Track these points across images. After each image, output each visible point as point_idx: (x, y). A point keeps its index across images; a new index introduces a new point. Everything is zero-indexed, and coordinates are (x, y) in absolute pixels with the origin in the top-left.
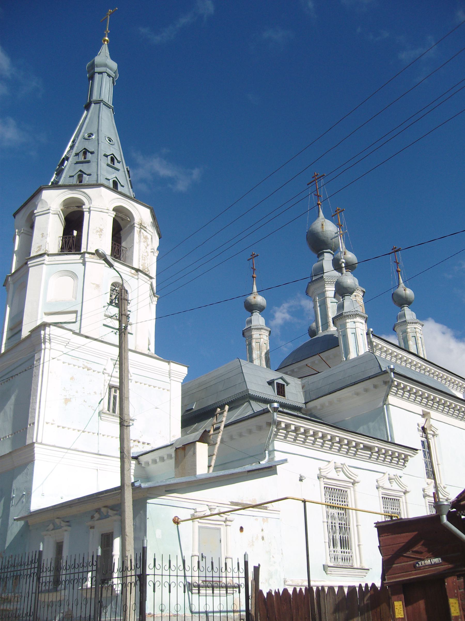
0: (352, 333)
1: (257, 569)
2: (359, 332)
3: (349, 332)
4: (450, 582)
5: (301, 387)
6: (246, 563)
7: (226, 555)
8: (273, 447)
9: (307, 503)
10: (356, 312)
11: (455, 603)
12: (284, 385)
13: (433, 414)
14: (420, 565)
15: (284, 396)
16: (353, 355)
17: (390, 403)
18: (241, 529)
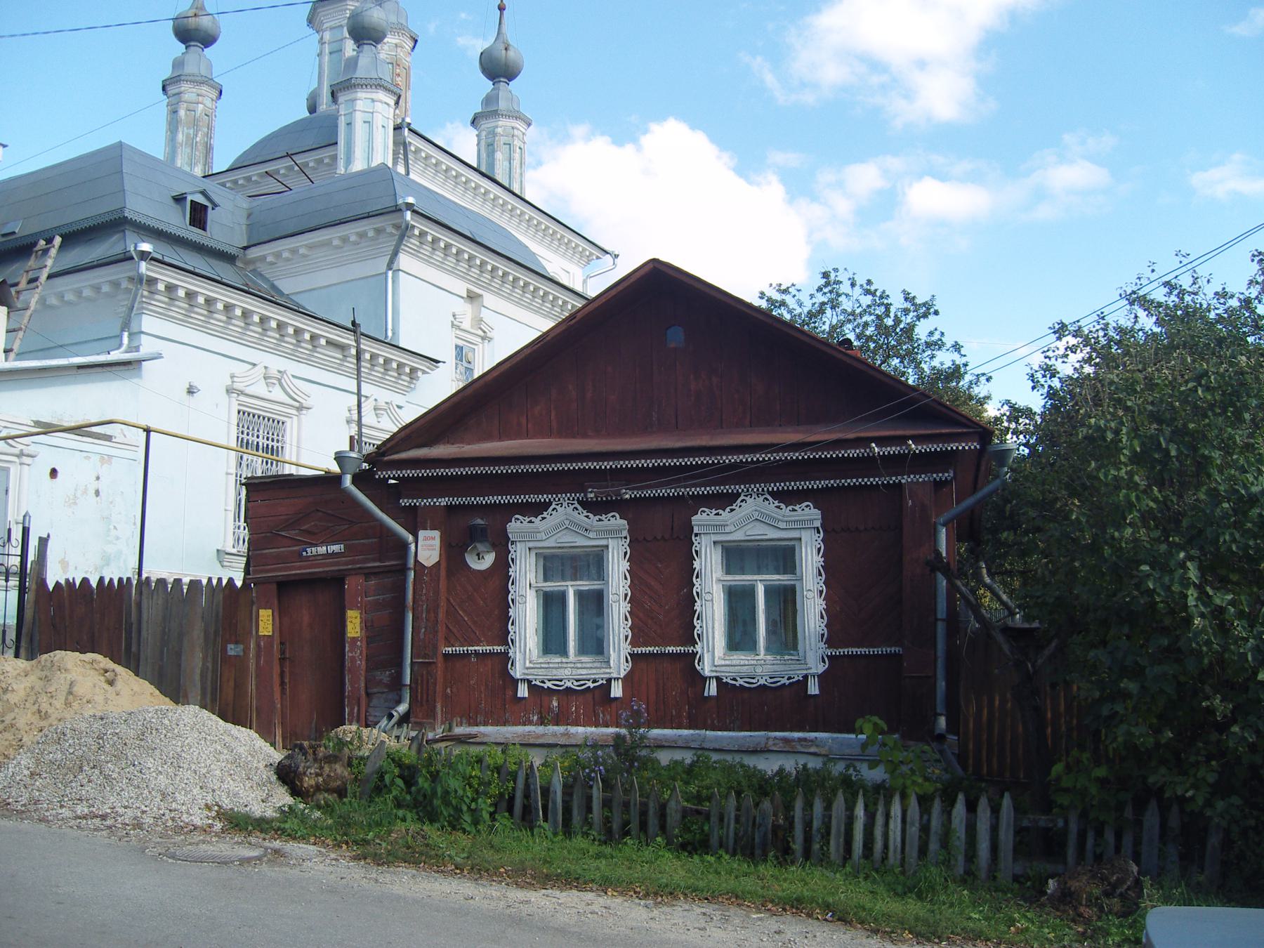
0: (365, 122)
1: (43, 542)
2: (379, 120)
3: (359, 118)
4: (352, 584)
5: (245, 215)
6: (26, 532)
7: (16, 517)
8: (140, 326)
9: (152, 433)
10: (379, 81)
11: (356, 618)
12: (206, 207)
13: (489, 299)
14: (309, 554)
15: (204, 229)
16: (358, 165)
17: (401, 268)
18: (54, 473)
